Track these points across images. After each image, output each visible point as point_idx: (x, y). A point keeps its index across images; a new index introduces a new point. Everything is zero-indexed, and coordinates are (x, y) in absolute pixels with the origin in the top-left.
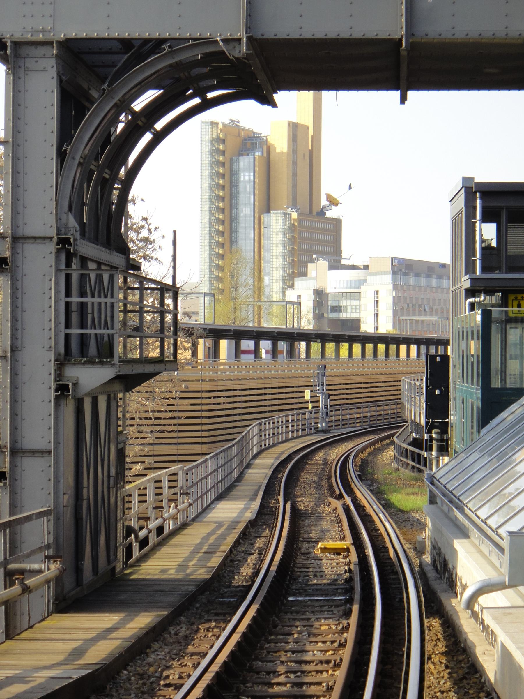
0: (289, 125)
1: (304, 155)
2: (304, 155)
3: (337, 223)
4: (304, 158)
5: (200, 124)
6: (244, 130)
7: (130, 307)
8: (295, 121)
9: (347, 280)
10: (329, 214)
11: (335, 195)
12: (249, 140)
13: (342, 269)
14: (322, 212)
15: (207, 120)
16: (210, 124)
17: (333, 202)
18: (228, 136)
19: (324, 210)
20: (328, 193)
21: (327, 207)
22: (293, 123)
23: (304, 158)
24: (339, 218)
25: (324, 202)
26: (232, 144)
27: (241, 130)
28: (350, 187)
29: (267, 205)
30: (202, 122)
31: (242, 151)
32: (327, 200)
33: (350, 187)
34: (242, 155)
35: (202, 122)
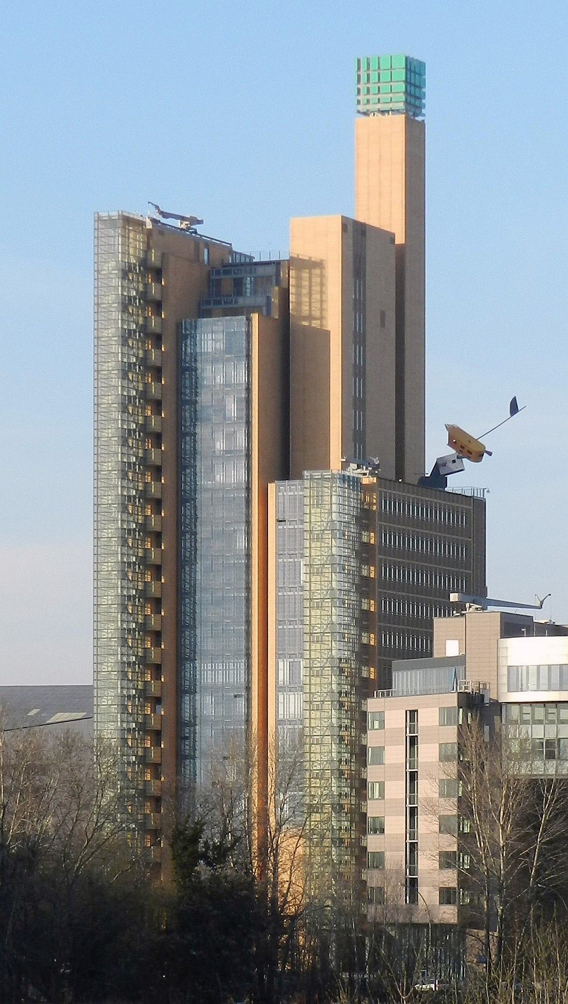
0: (344, 227)
1: (383, 315)
2: (383, 315)
3: (475, 508)
4: (383, 324)
5: (91, 224)
6: (209, 244)
7: (312, 755)
8: (361, 220)
9: (538, 667)
10: (455, 483)
11: (473, 430)
12: (227, 272)
13: (529, 634)
14: (439, 477)
15: (114, 214)
16: (120, 223)
17: (467, 448)
18: (172, 259)
19: (442, 471)
20: (451, 423)
21: (450, 465)
22: (356, 223)
23: (383, 324)
24: (478, 495)
25: (436, 448)
26: (178, 283)
27: (202, 245)
28: (514, 408)
29: (286, 454)
30: (99, 219)
31: (208, 303)
32: (452, 443)
33: (514, 408)
34: (208, 314)
35: (99, 219)
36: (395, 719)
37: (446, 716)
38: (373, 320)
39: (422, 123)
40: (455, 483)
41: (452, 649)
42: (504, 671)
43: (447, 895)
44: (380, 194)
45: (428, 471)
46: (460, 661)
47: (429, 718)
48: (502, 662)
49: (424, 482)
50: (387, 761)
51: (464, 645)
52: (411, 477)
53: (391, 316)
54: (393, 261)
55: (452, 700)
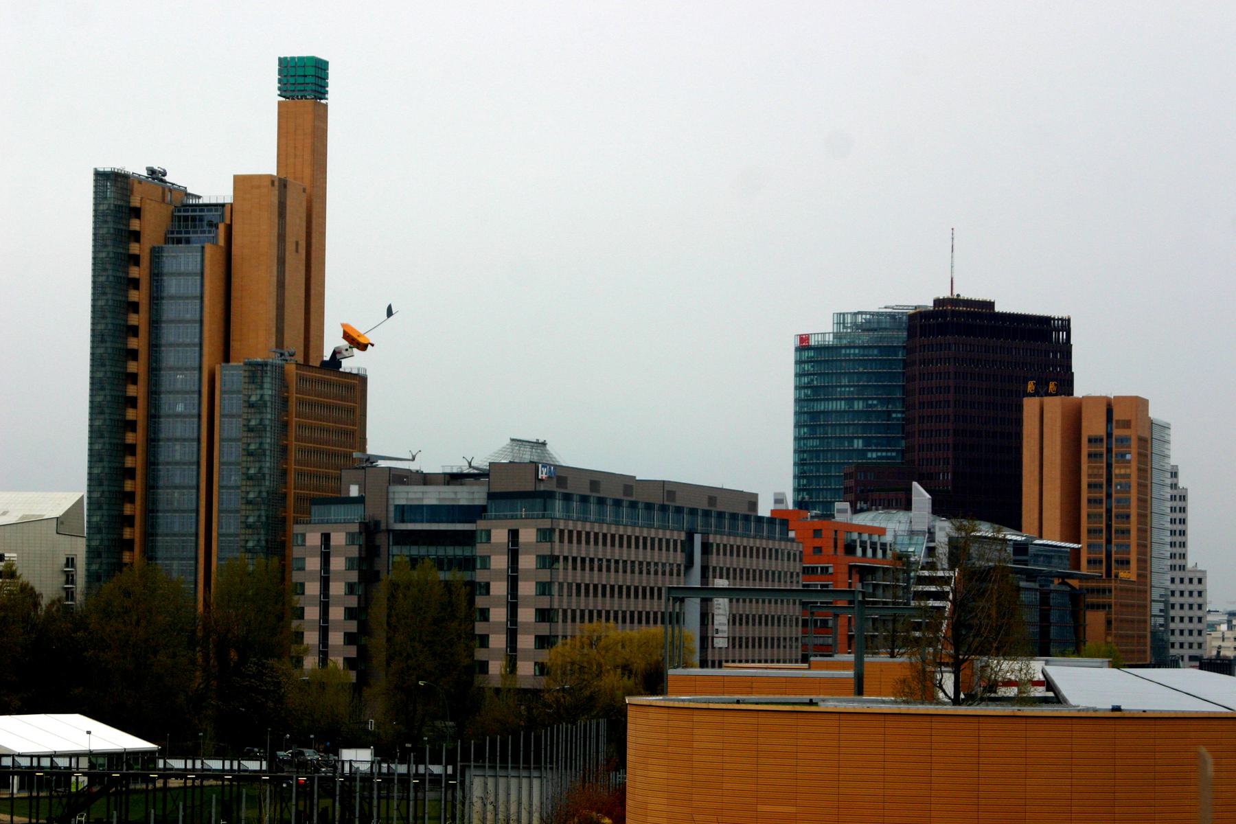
1: (297, 244)
2: (297, 244)
3: (360, 381)
4: (297, 251)
10: (347, 365)
17: (355, 342)
19: (338, 356)
20: (345, 322)
23: (297, 251)
24: (362, 372)
25: (332, 340)
28: (390, 313)
33: (390, 313)
36: (314, 539)
37: (351, 538)
38: (290, 247)
39: (326, 106)
40: (347, 365)
41: (354, 491)
42: (392, 509)
43: (350, 663)
44: (295, 155)
45: (327, 356)
46: (360, 500)
47: (338, 539)
48: (391, 502)
49: (324, 364)
50: (492, 619)
51: (363, 488)
52: (315, 362)
53: (303, 244)
54: (304, 204)
55: (355, 528)
